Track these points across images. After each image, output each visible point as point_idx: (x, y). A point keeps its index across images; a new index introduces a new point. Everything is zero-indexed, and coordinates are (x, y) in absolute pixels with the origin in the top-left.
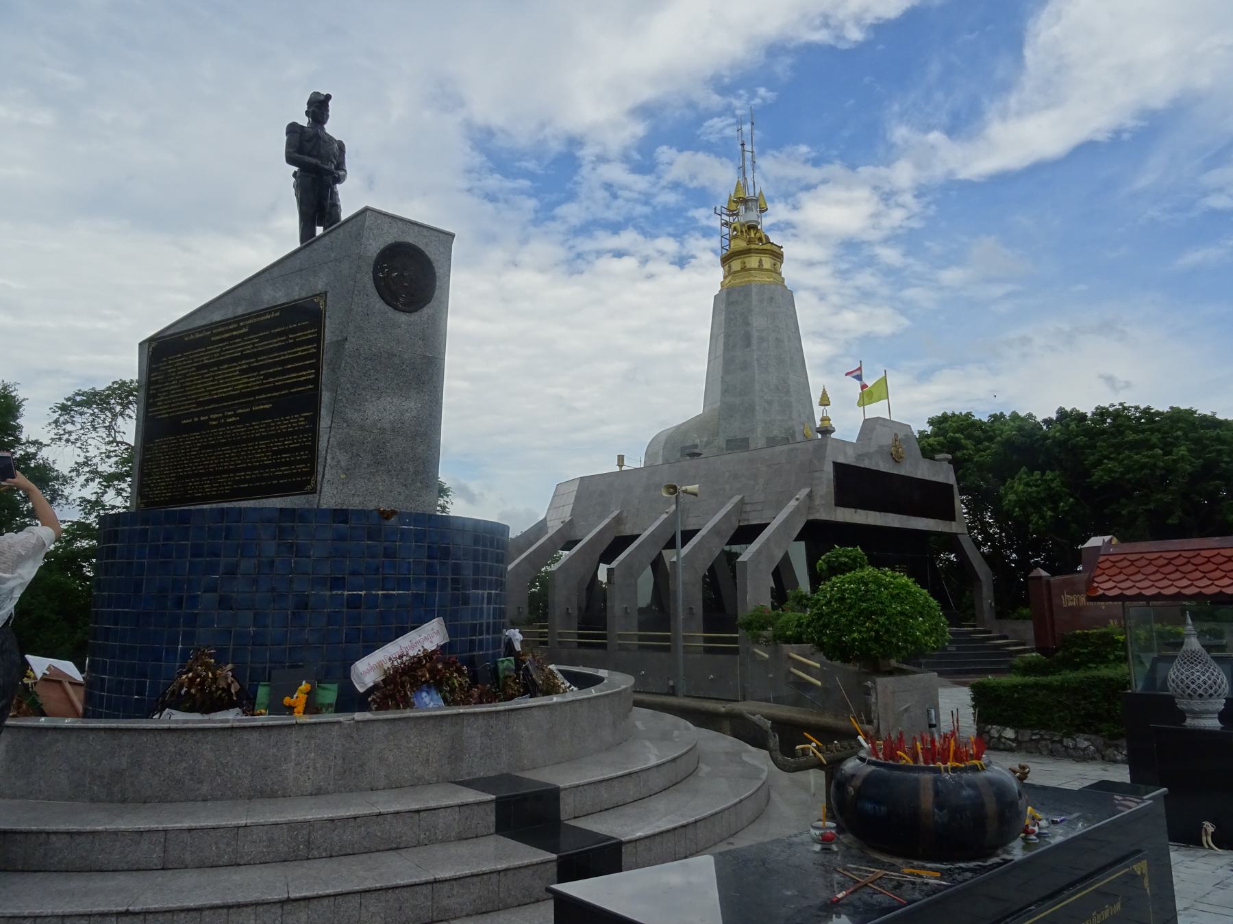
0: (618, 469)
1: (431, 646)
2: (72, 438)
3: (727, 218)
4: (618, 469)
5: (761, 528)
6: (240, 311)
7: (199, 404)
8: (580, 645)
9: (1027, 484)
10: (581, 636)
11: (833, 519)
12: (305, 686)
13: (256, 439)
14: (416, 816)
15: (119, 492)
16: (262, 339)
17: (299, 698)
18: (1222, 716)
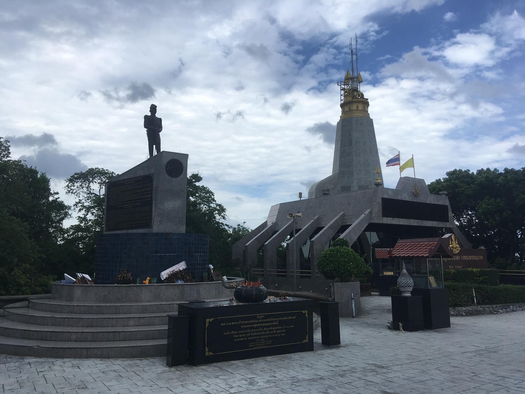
0: (299, 199)
1: (181, 269)
2: (74, 191)
3: (343, 86)
6: (132, 176)
8: (278, 276)
9: (488, 205)
10: (278, 272)
11: (381, 222)
12: (148, 278)
15: (93, 214)
17: (147, 282)
18: (411, 293)
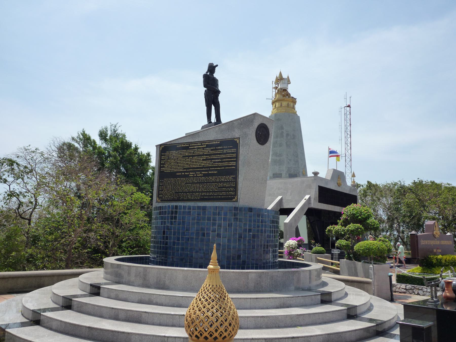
7: (185, 169)
13: (210, 182)
16: (212, 150)
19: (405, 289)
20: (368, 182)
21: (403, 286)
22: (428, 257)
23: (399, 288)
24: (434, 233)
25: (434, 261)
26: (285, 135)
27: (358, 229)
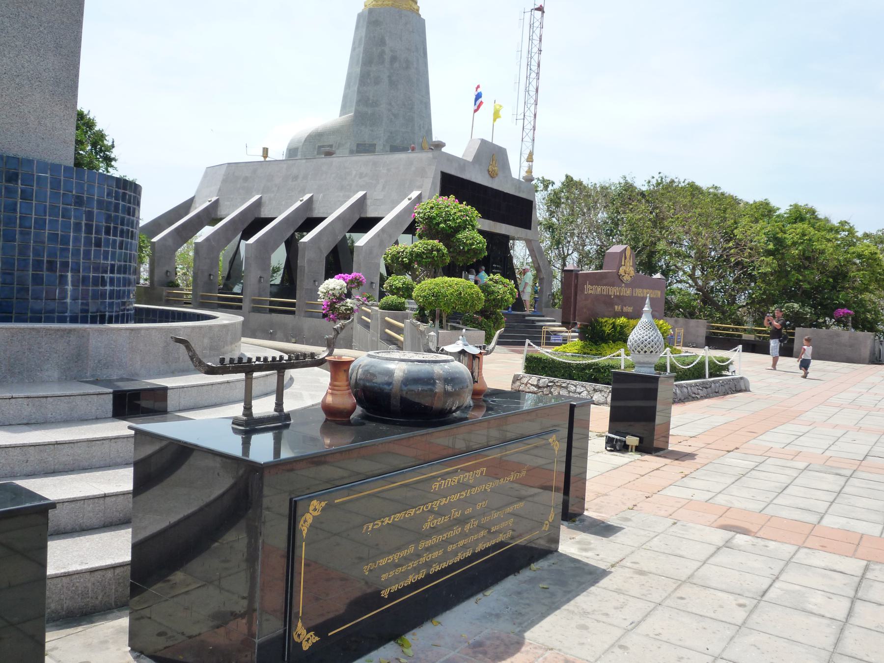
0: (262, 159)
4: (262, 159)
5: (376, 220)
14: (101, 501)
19: (537, 386)
20: (567, 177)
21: (534, 379)
22: (597, 321)
23: (526, 385)
24: (621, 271)
25: (608, 329)
26: (387, 58)
27: (432, 250)
